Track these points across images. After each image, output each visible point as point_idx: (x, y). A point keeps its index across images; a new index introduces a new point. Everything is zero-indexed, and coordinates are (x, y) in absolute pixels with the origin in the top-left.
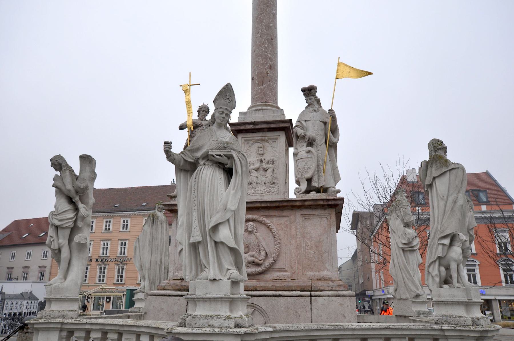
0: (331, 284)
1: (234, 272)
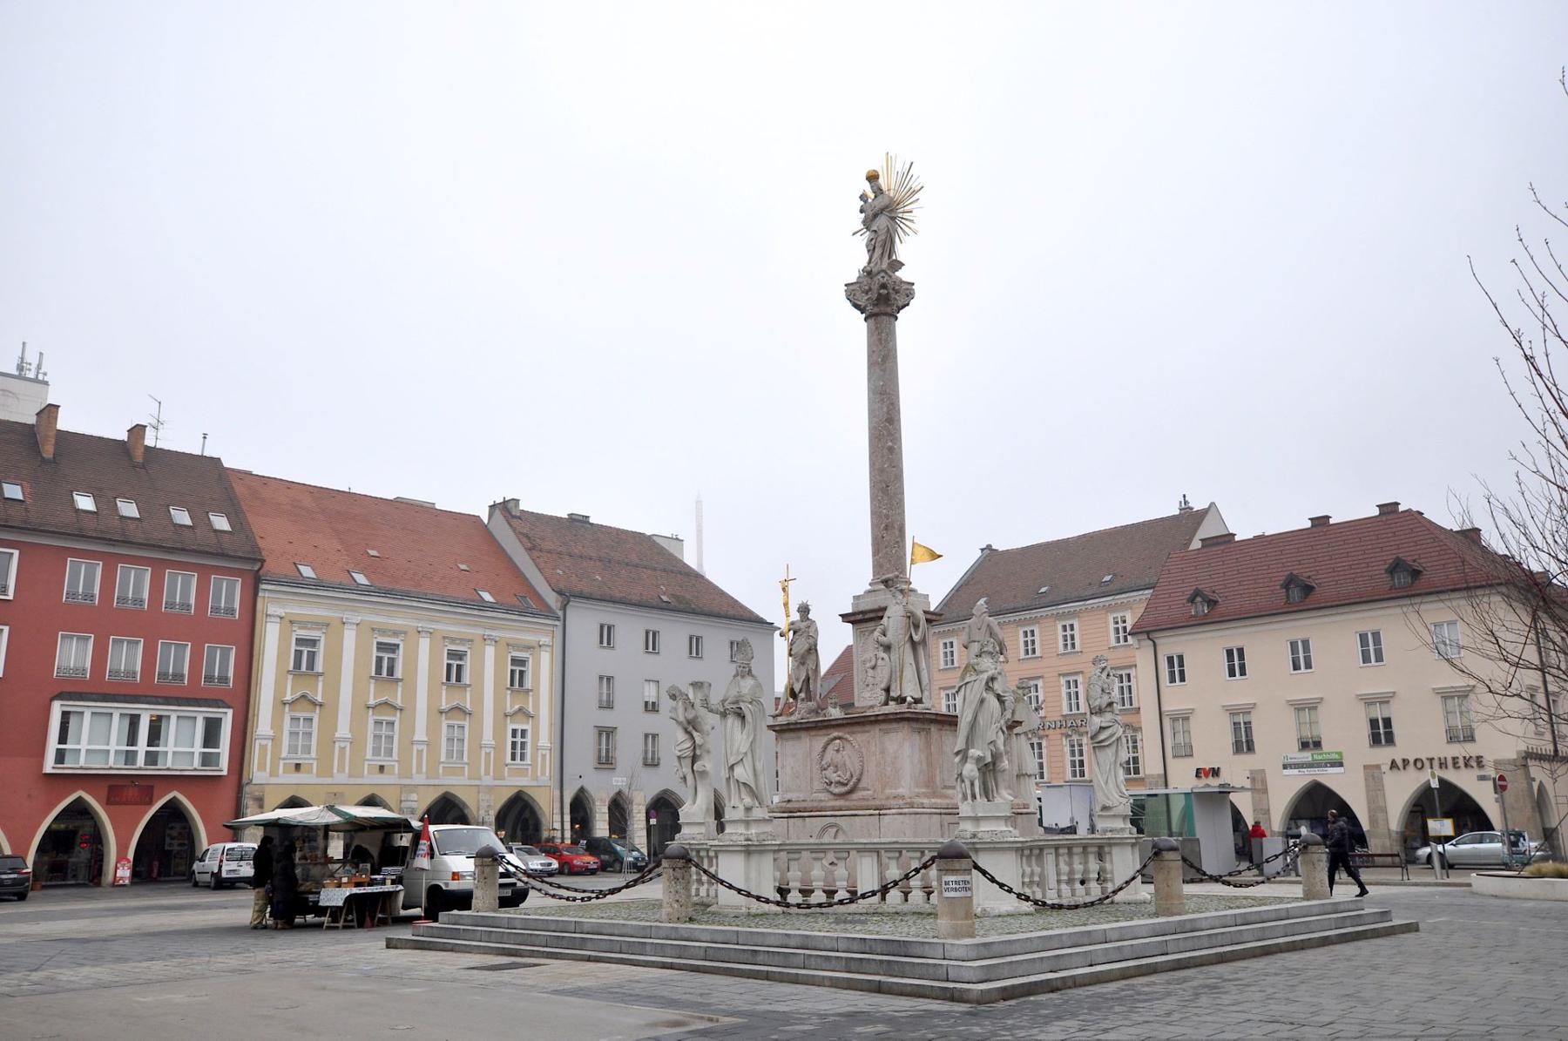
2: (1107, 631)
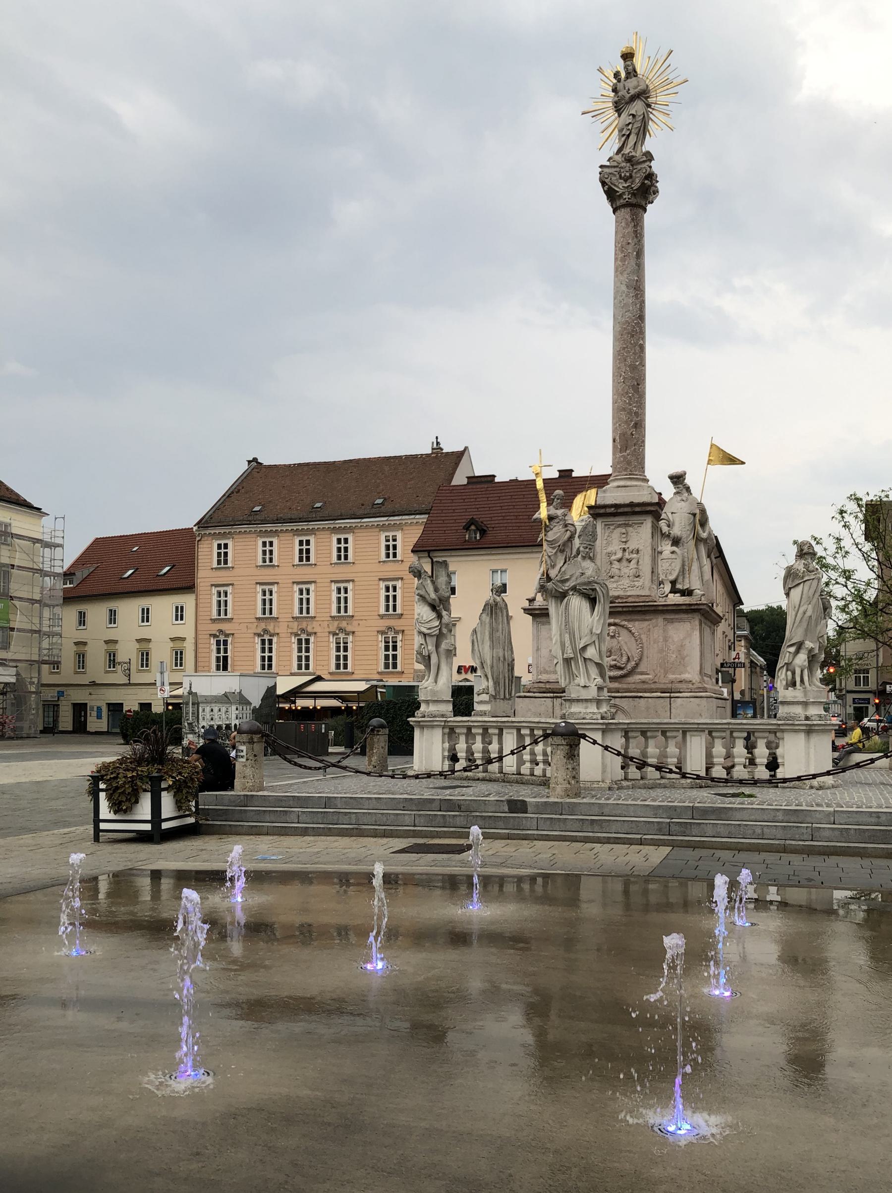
0: (690, 686)
1: (599, 680)
2: (379, 547)
